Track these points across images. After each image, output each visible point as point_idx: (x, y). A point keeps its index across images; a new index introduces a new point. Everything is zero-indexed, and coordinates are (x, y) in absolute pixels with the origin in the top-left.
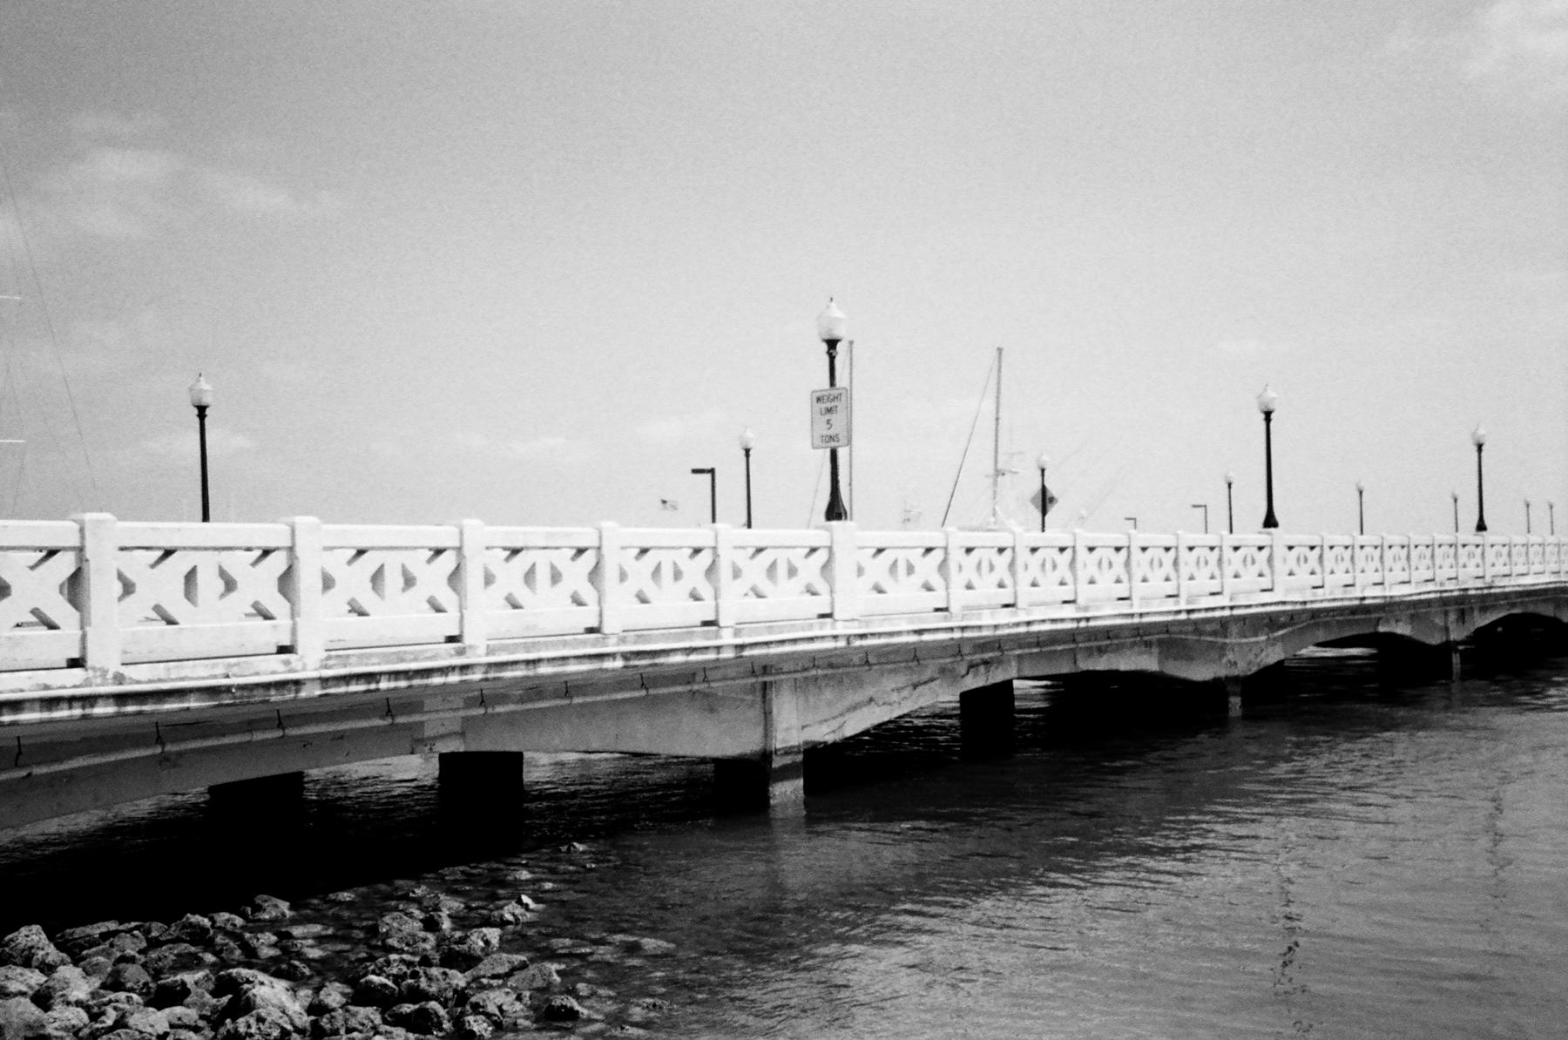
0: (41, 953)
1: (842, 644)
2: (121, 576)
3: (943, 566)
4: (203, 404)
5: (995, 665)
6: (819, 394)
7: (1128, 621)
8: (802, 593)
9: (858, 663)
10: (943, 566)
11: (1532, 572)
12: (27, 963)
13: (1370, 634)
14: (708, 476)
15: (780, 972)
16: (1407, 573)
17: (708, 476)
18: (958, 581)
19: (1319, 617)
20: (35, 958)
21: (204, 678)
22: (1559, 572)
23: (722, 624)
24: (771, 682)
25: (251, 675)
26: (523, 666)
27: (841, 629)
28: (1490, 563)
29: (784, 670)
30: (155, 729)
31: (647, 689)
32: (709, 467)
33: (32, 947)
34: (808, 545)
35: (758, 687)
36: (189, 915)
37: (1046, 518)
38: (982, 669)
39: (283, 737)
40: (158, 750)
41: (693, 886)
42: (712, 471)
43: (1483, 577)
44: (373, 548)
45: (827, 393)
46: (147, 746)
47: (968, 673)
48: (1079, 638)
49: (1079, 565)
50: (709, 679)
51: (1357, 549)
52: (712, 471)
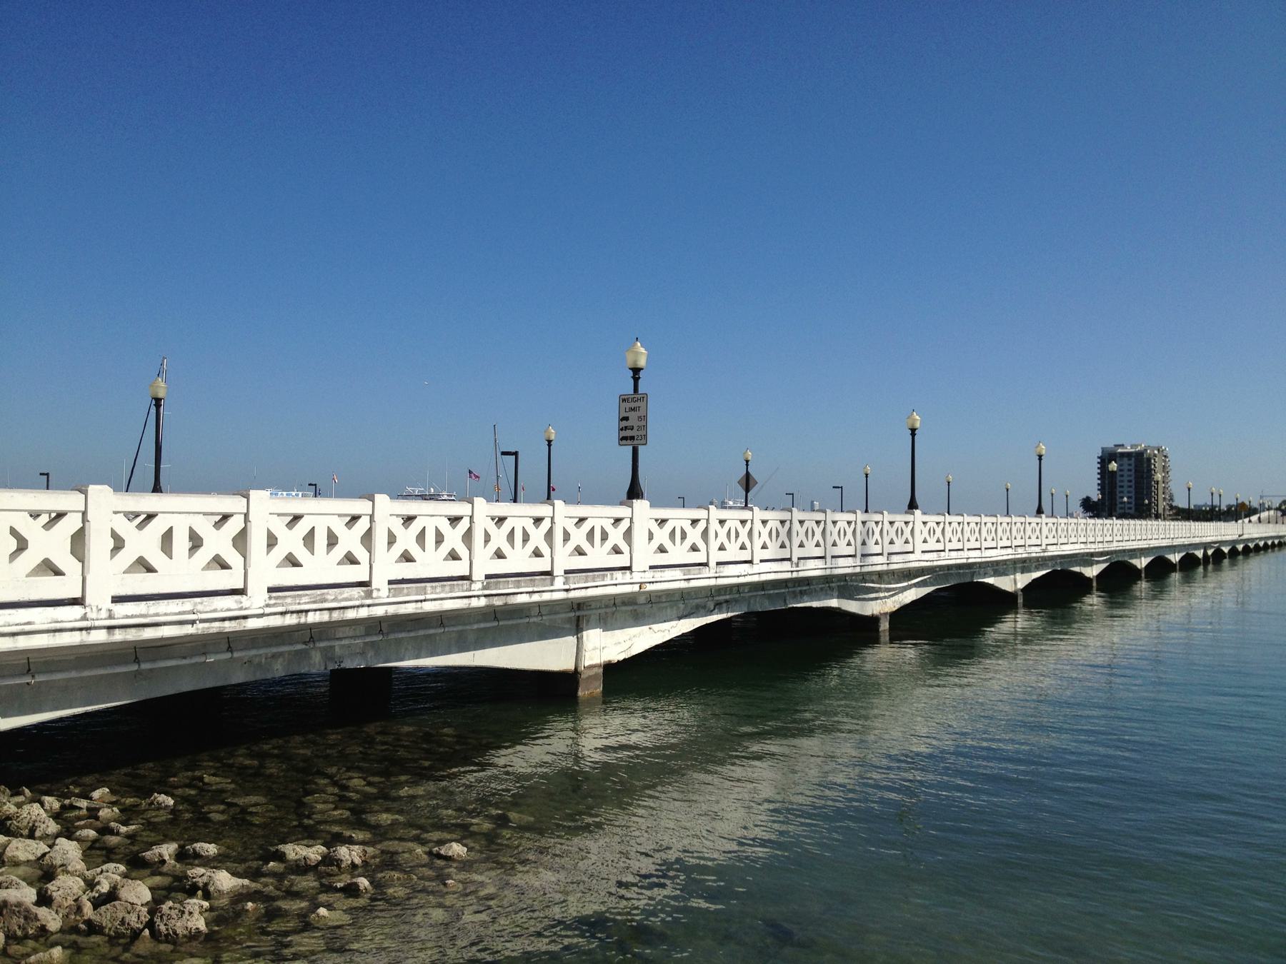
0: (43, 826)
1: (636, 588)
2: (13, 532)
3: (705, 534)
4: (639, 366)
5: (734, 603)
6: (623, 397)
7: (188, 630)
8: (530, 557)
9: (645, 602)
10: (705, 534)
11: (1079, 541)
12: (31, 836)
13: (969, 582)
14: (46, 476)
15: (236, 865)
16: (1010, 541)
17: (46, 476)
18: (714, 545)
19: (952, 570)
20: (38, 829)
21: (132, 617)
22: (1086, 543)
23: (474, 579)
24: (583, 616)
25: (211, 612)
26: (104, 631)
27: (637, 577)
28: (1045, 536)
29: (592, 607)
30: (27, 661)
31: (498, 621)
32: (514, 451)
33: (35, 821)
34: (578, 516)
35: (574, 620)
36: (156, 794)
37: (444, 517)
38: (724, 605)
39: (231, 658)
40: (135, 667)
41: (1059, 682)
42: (516, 454)
43: (1041, 545)
44: (235, 513)
45: (631, 396)
46: (126, 663)
47: (714, 609)
48: (789, 585)
49: (794, 534)
50: (543, 613)
51: (1027, 525)
52: (516, 454)
